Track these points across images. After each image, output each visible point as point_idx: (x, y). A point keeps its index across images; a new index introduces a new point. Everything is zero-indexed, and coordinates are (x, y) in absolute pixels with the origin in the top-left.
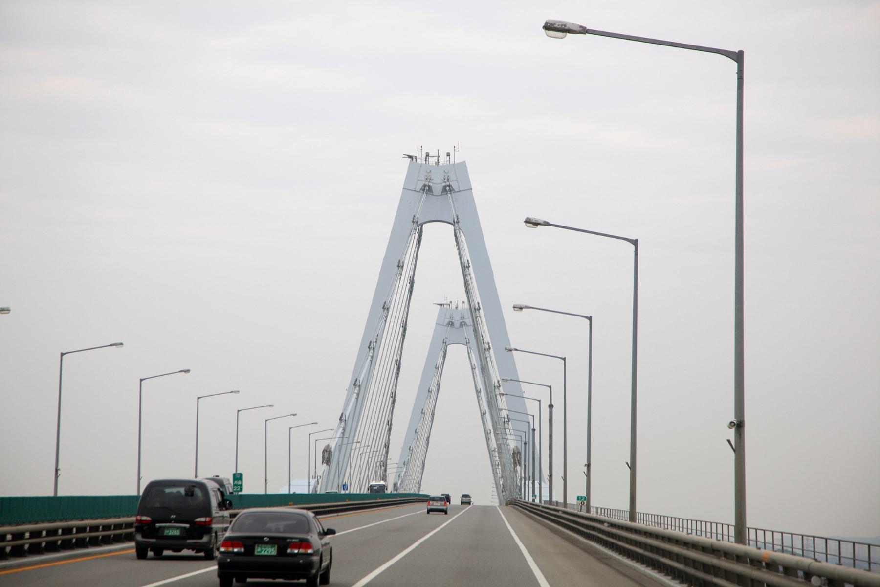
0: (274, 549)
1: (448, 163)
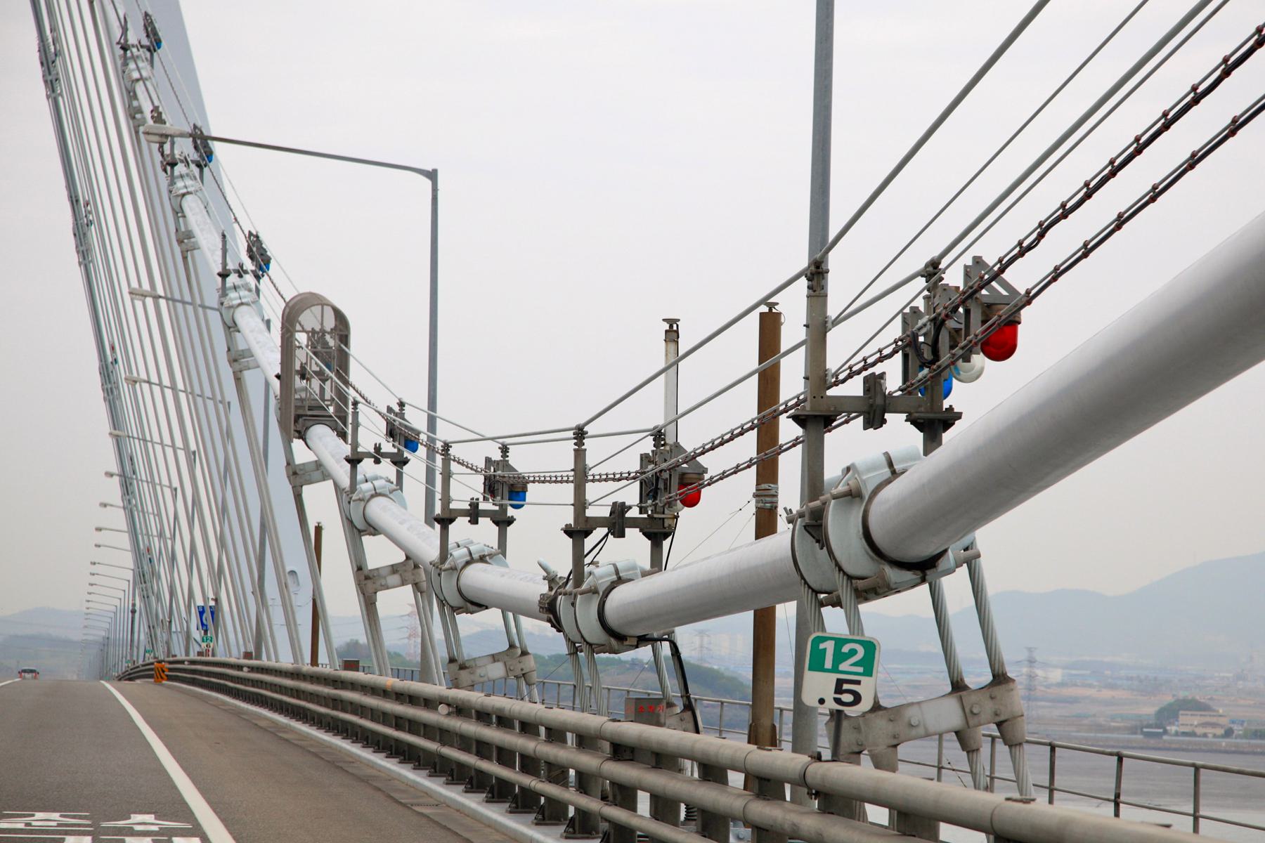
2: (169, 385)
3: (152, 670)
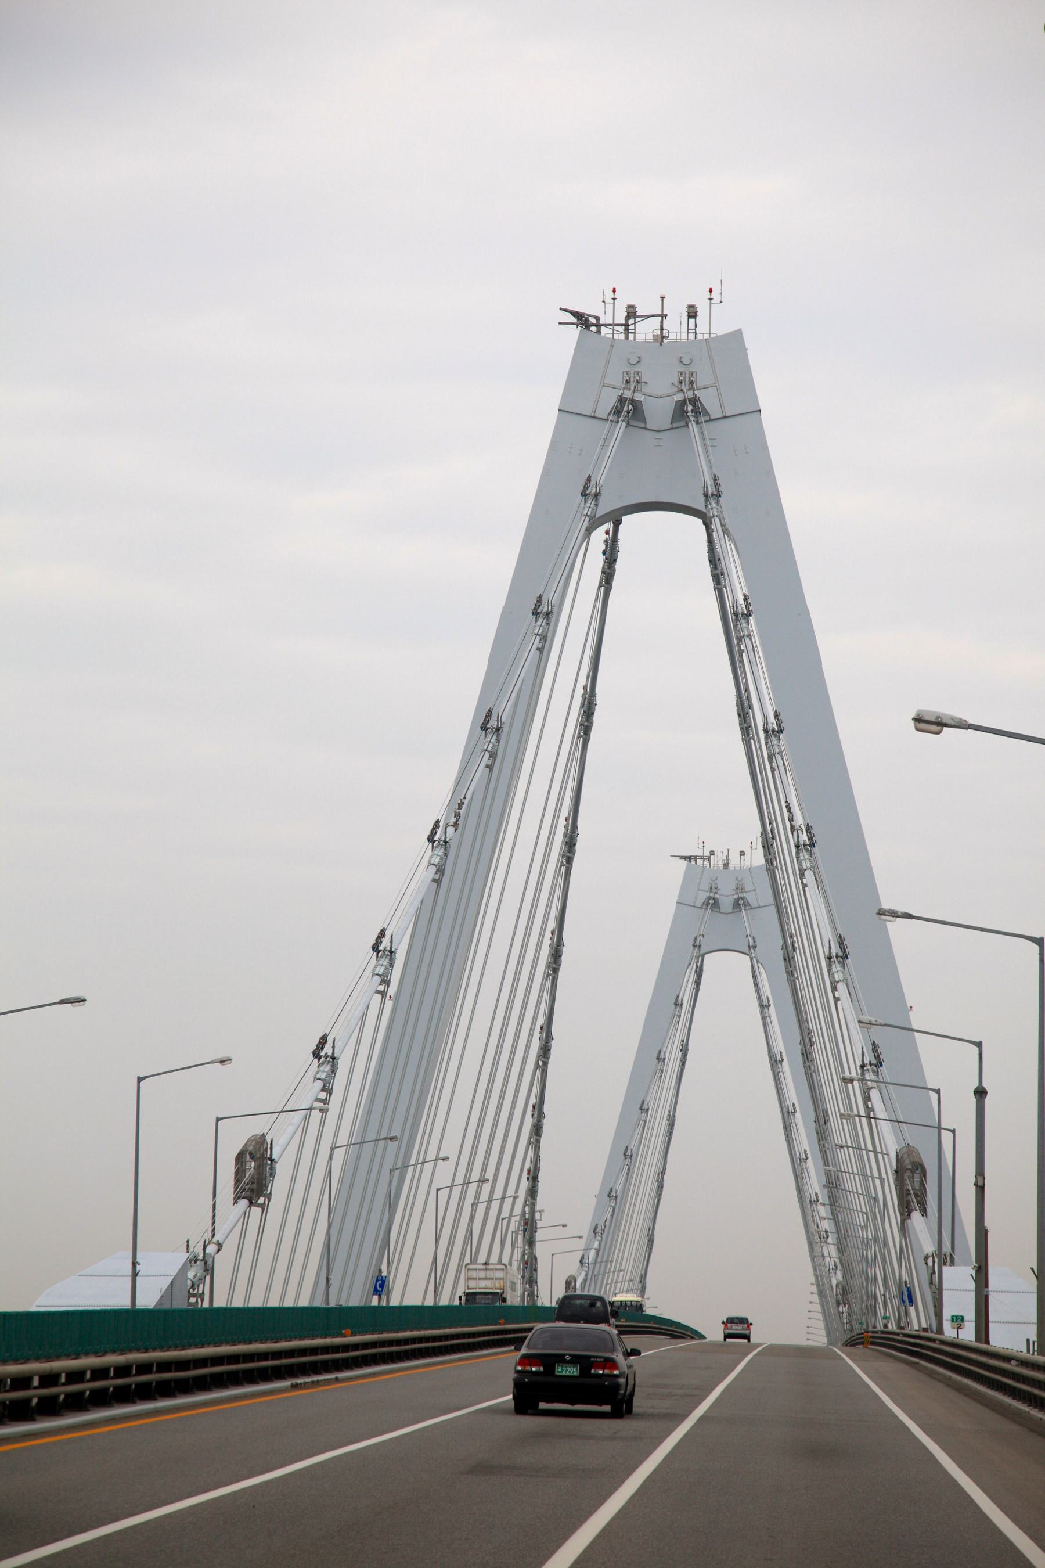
0: (577, 1370)
1: (692, 337)
2: (872, 1150)
3: (863, 1338)
